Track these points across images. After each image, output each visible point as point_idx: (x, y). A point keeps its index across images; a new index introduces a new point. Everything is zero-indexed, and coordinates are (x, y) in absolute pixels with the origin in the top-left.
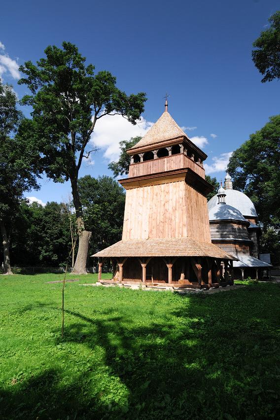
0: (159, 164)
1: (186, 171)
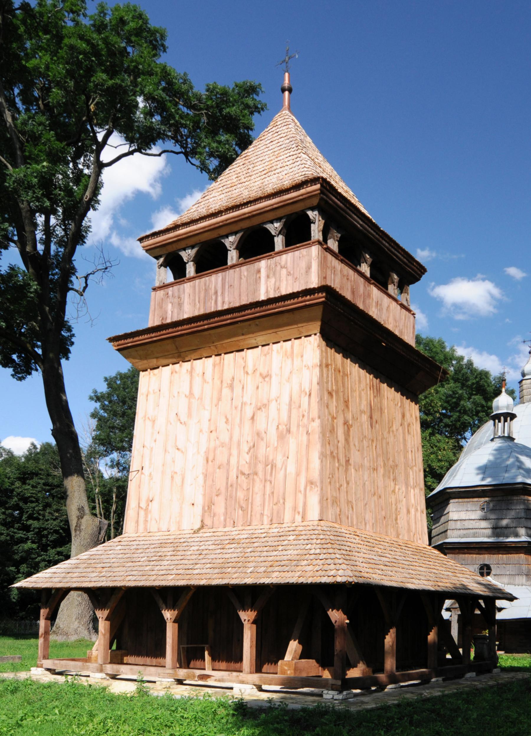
0: (244, 280)
1: (321, 297)
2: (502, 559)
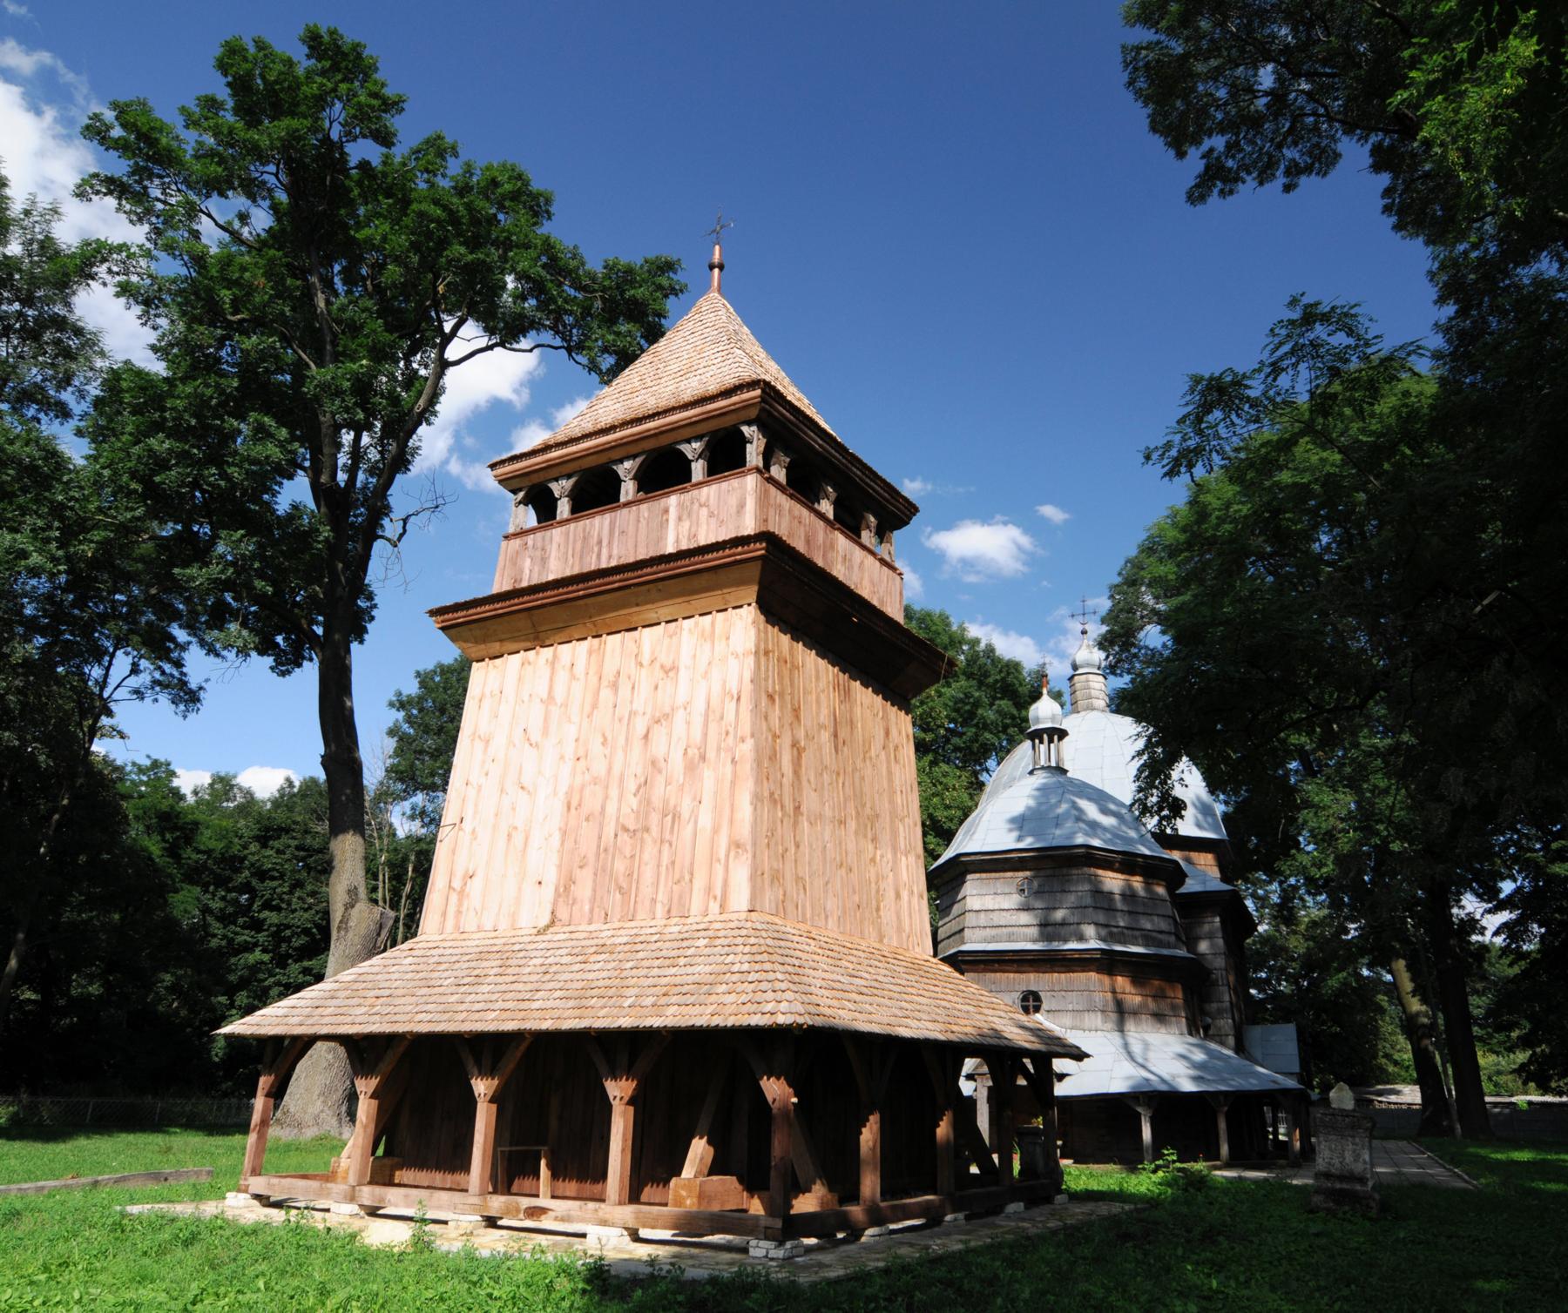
0: (643, 523)
1: (759, 549)
2: (1059, 982)
